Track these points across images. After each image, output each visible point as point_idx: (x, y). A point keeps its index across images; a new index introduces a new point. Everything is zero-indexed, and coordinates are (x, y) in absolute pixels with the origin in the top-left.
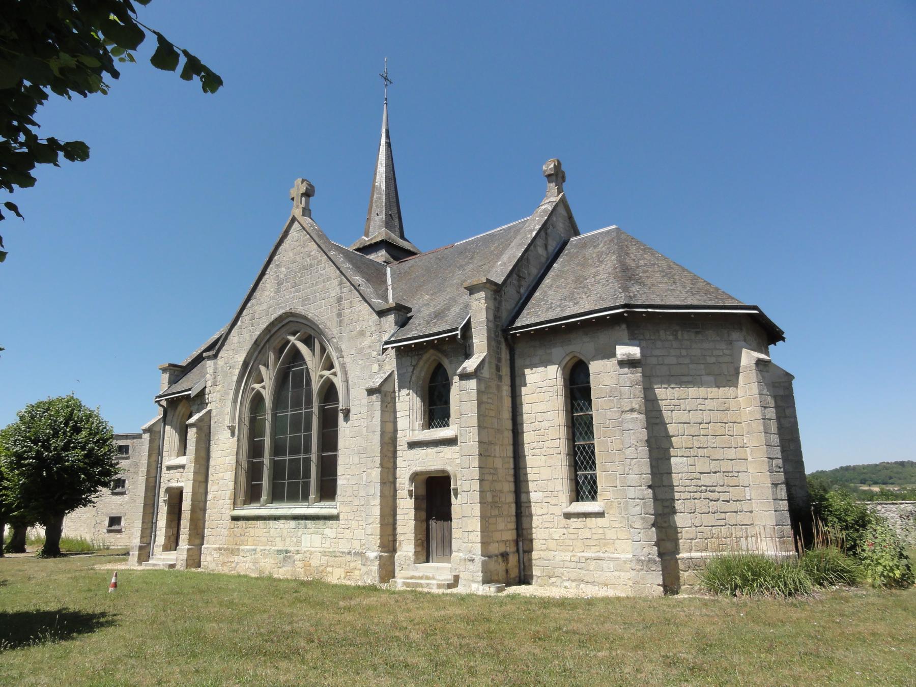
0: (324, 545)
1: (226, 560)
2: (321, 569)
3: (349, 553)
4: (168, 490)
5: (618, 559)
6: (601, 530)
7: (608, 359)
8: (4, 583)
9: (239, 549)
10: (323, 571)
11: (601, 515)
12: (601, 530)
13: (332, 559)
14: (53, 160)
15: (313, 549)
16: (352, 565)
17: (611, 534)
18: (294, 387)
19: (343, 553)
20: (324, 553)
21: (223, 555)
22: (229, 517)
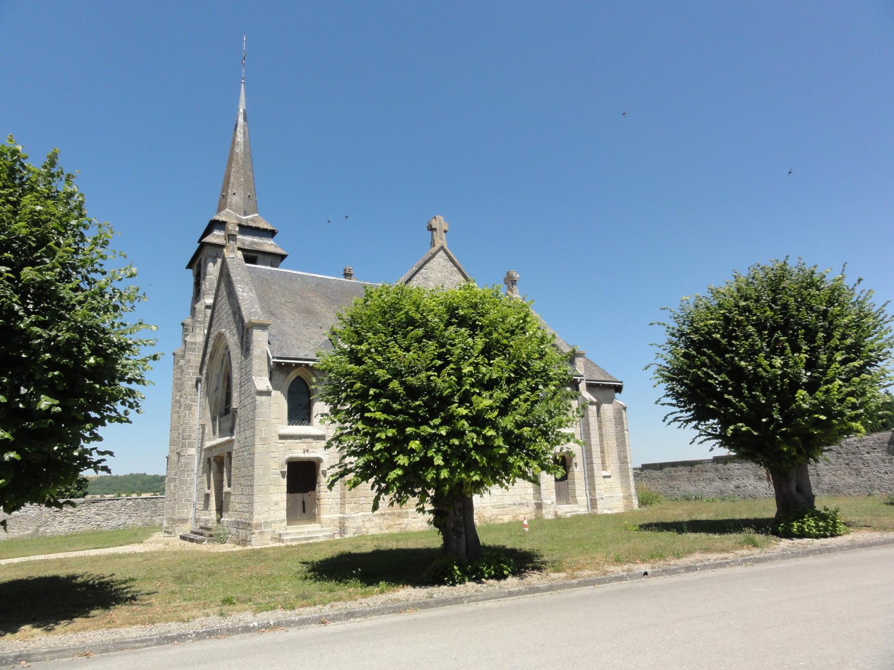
0: (492, 501)
1: (392, 523)
2: (493, 518)
3: (515, 504)
4: (257, 257)
5: (617, 496)
6: (610, 484)
7: (350, 553)
8: (892, 504)
9: (407, 513)
10: (495, 519)
11: (609, 477)
12: (610, 484)
13: (502, 509)
14: (104, 425)
15: (485, 505)
16: (518, 512)
17: (614, 485)
18: (311, 534)
19: (510, 505)
20: (494, 507)
21: (388, 519)
22: (297, 567)
